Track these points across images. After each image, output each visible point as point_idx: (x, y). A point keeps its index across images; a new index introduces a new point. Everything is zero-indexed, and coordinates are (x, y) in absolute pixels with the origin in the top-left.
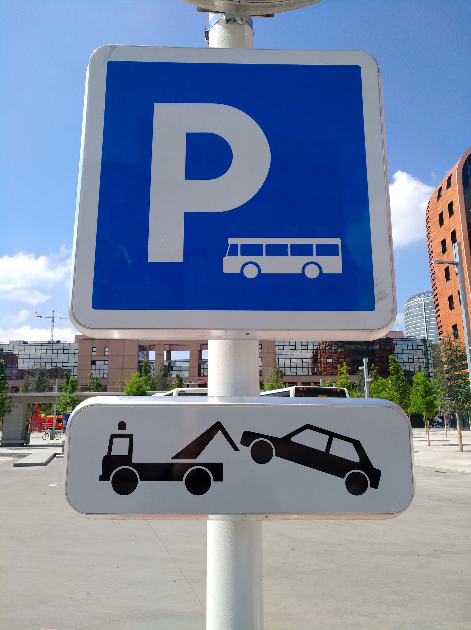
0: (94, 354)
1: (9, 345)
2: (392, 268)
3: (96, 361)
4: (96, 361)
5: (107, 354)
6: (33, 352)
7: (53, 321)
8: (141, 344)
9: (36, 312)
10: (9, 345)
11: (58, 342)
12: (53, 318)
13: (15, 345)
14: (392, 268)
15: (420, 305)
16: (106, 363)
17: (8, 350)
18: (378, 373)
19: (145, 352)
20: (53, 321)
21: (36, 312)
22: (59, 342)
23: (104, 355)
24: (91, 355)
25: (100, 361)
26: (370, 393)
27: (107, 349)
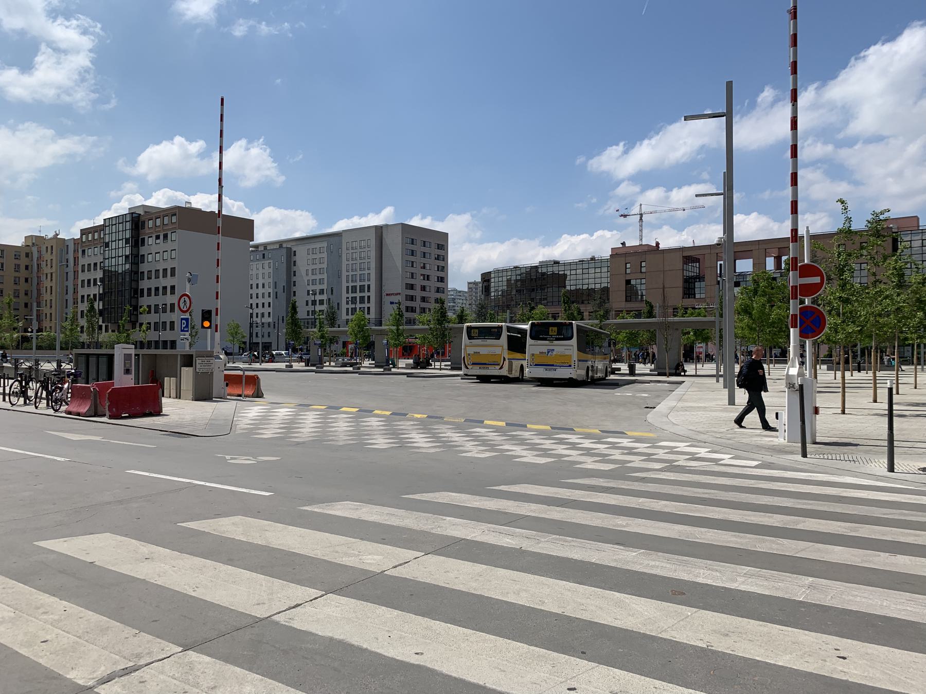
0: (628, 271)
1: (590, 262)
2: (865, 531)
3: (630, 280)
4: (630, 280)
5: (644, 270)
6: (598, 270)
7: (641, 219)
8: (686, 254)
9: (617, 211)
10: (590, 262)
11: (593, 259)
12: (641, 215)
13: (913, 232)
14: (865, 531)
15: (354, 279)
16: (643, 281)
17: (559, 271)
18: (239, 30)
19: (698, 264)
20: (641, 219)
21: (617, 211)
22: (593, 258)
23: (640, 271)
24: (625, 273)
25: (636, 279)
26: (410, 323)
27: (643, 264)
